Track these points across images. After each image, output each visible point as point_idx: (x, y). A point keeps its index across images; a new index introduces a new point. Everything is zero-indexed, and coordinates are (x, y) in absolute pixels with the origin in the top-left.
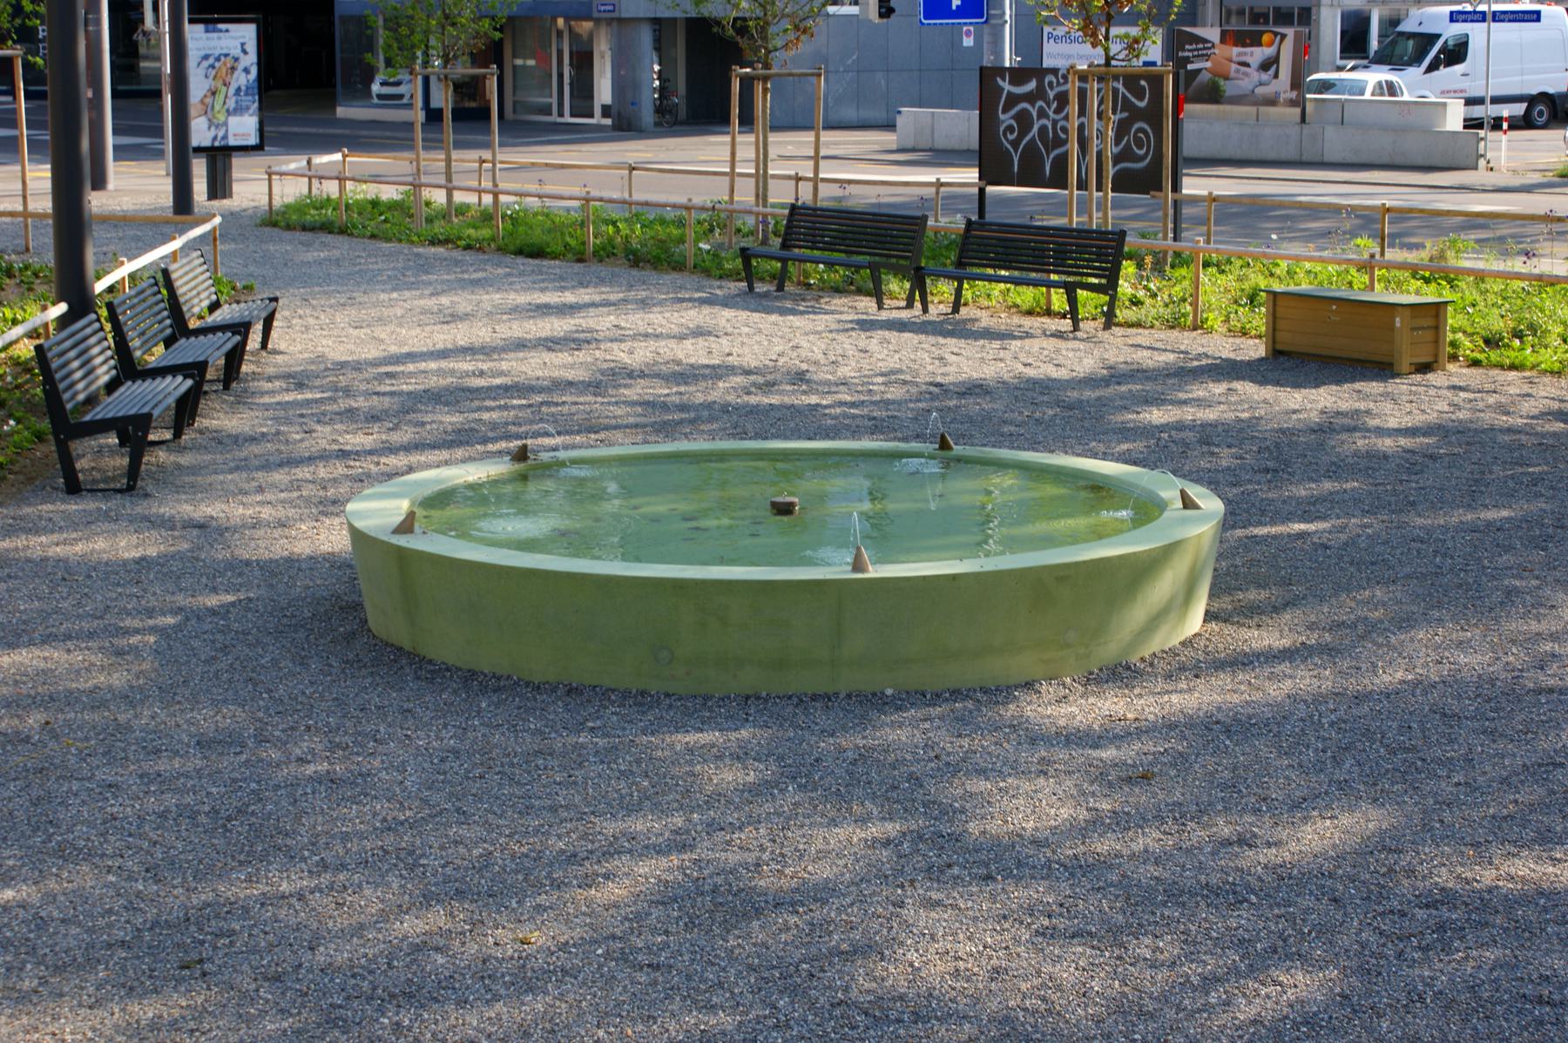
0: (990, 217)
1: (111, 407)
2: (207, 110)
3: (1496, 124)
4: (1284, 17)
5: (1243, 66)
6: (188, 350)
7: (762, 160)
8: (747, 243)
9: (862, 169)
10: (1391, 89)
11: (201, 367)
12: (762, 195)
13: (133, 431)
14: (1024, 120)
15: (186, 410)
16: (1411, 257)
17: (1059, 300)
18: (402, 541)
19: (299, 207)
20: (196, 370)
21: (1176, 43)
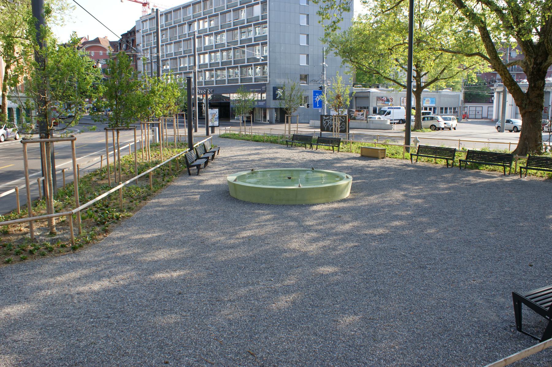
0: (322, 136)
1: (195, 163)
2: (211, 121)
3: (394, 123)
4: (365, 108)
5: (358, 115)
6: (207, 155)
7: (290, 128)
8: (287, 140)
9: (304, 129)
10: (380, 118)
11: (208, 157)
12: (289, 133)
13: (198, 166)
14: (327, 122)
15: (206, 163)
16: (382, 142)
17: (331, 148)
18: (234, 182)
19: (224, 135)
20: (208, 158)
21: (349, 111)
